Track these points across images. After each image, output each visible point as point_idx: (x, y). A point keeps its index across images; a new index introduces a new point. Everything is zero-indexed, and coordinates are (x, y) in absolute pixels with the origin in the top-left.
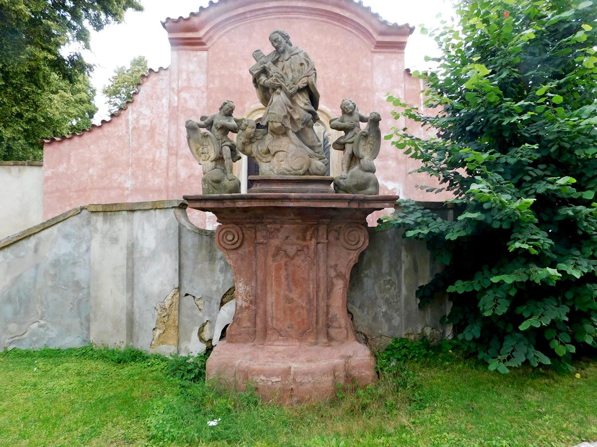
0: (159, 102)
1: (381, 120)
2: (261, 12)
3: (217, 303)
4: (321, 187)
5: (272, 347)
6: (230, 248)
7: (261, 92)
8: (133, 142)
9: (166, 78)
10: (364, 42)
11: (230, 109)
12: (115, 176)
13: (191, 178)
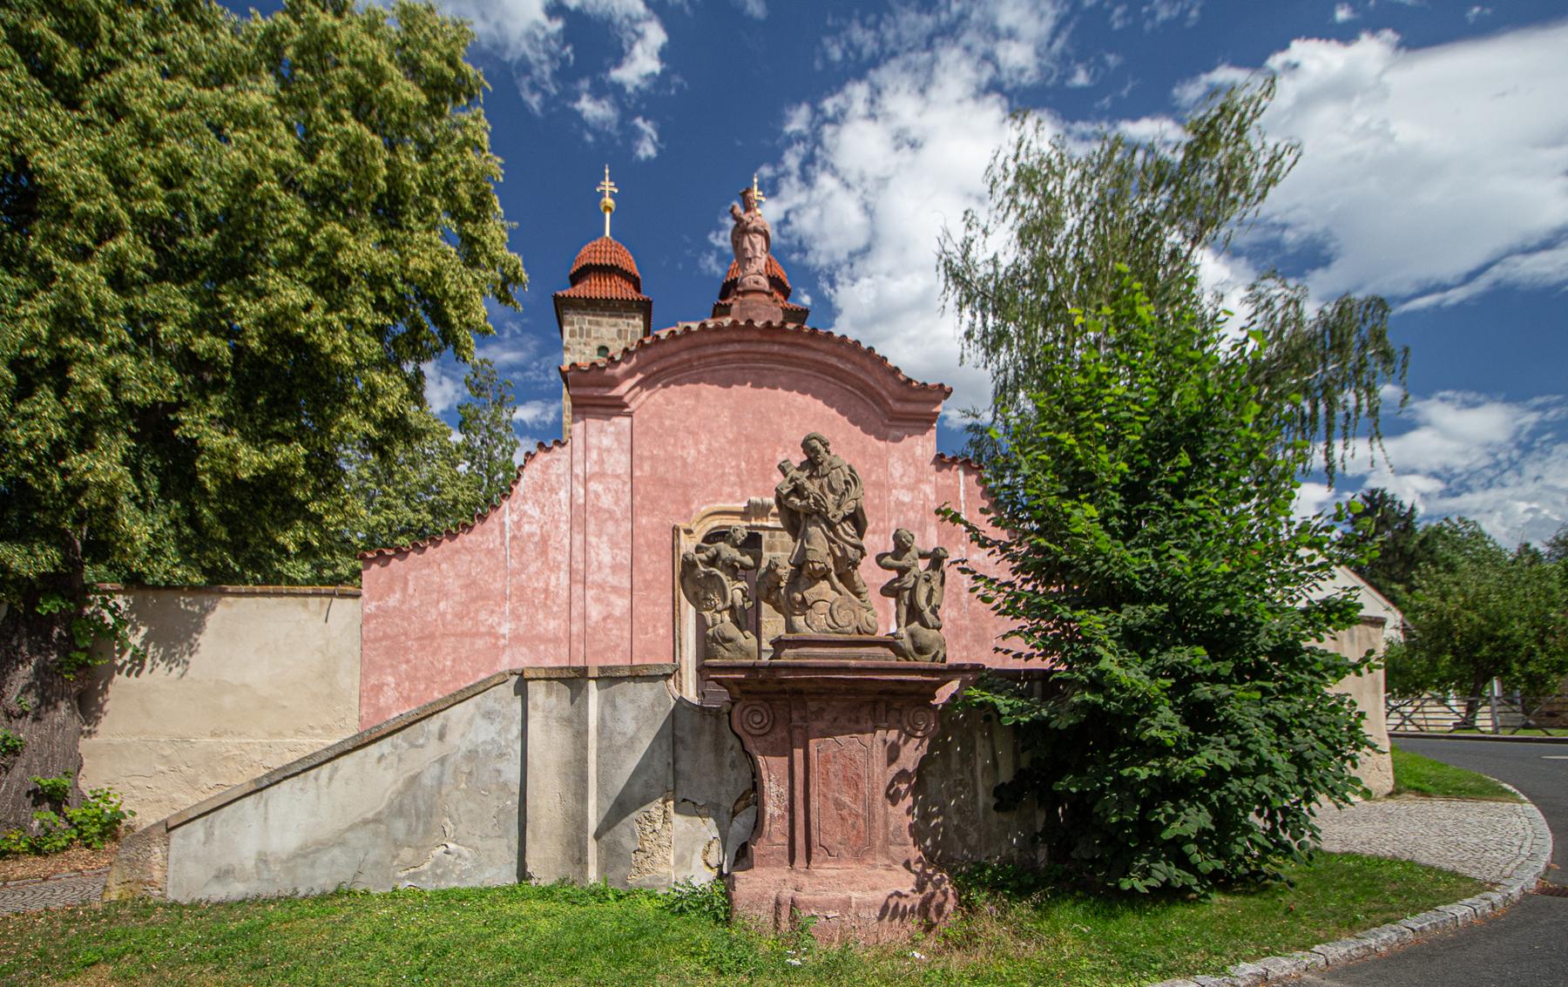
2: (715, 359)
9: (566, 457)
12: (483, 615)
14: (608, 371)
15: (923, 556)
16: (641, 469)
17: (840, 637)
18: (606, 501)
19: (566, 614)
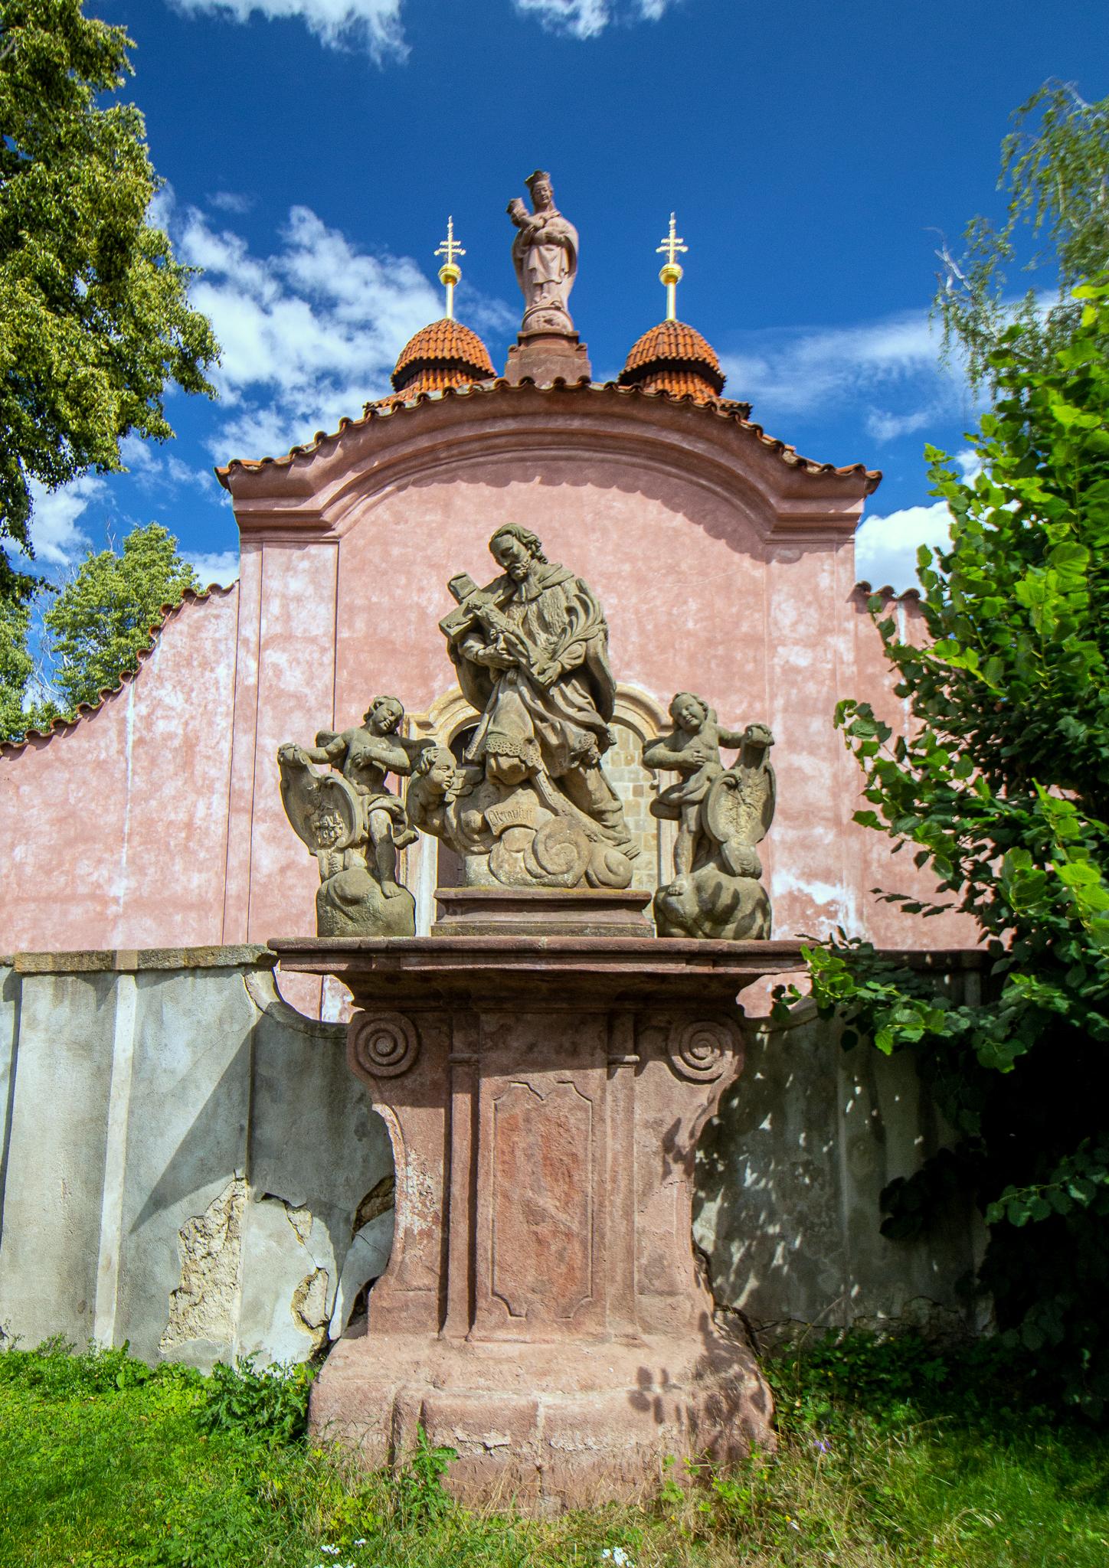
0: (207, 674)
1: (772, 744)
2: (476, 446)
3: (347, 1220)
4: (623, 917)
5: (489, 1345)
6: (385, 1073)
7: (469, 678)
8: (137, 779)
9: (229, 612)
10: (747, 517)
11: (392, 718)
12: (84, 867)
13: (289, 873)
14: (295, 472)
15: (726, 742)
16: (351, 627)
17: (546, 893)
18: (293, 680)
19: (220, 863)
